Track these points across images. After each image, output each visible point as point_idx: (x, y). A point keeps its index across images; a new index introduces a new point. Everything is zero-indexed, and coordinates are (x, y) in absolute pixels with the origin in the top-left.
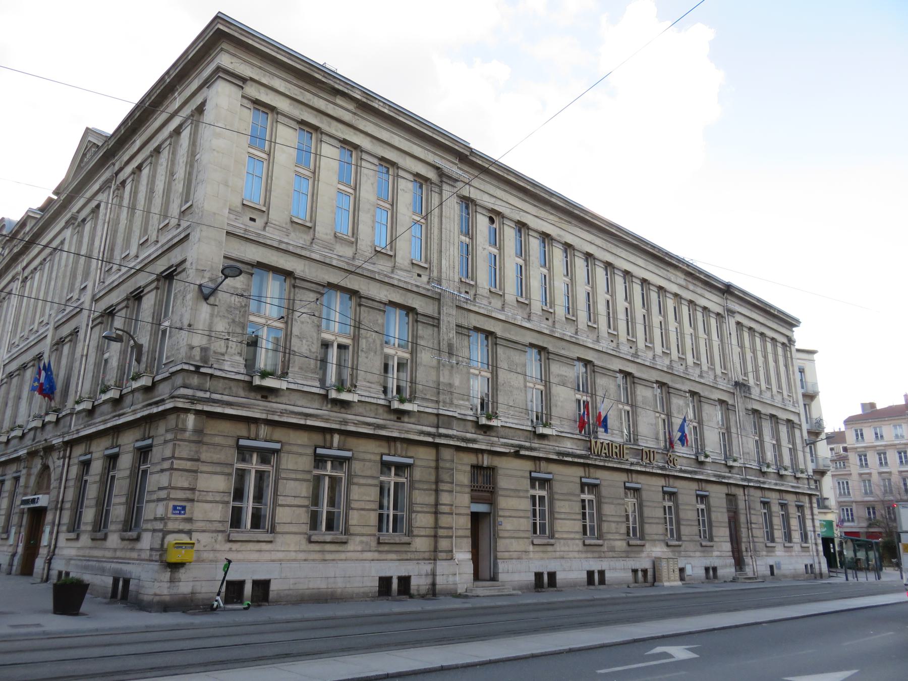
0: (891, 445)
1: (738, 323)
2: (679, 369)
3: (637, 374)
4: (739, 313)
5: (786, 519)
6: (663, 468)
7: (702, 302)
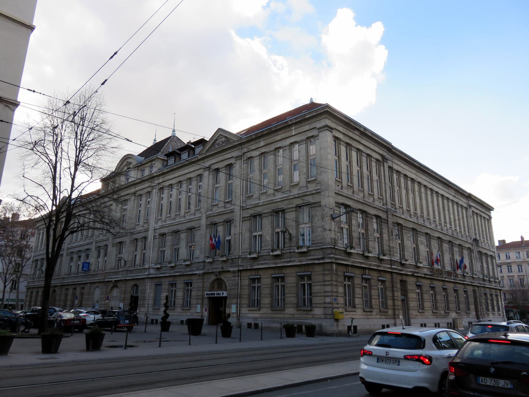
0: (514, 262)
1: (473, 211)
2: (455, 235)
3: (443, 238)
4: (473, 207)
5: (492, 300)
6: (454, 279)
7: (419, 180)
